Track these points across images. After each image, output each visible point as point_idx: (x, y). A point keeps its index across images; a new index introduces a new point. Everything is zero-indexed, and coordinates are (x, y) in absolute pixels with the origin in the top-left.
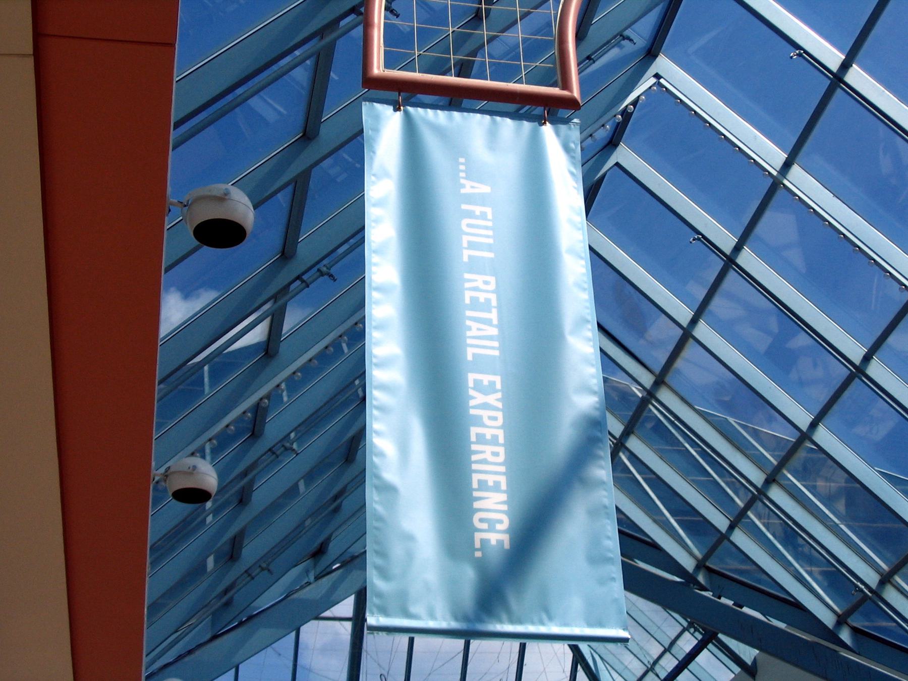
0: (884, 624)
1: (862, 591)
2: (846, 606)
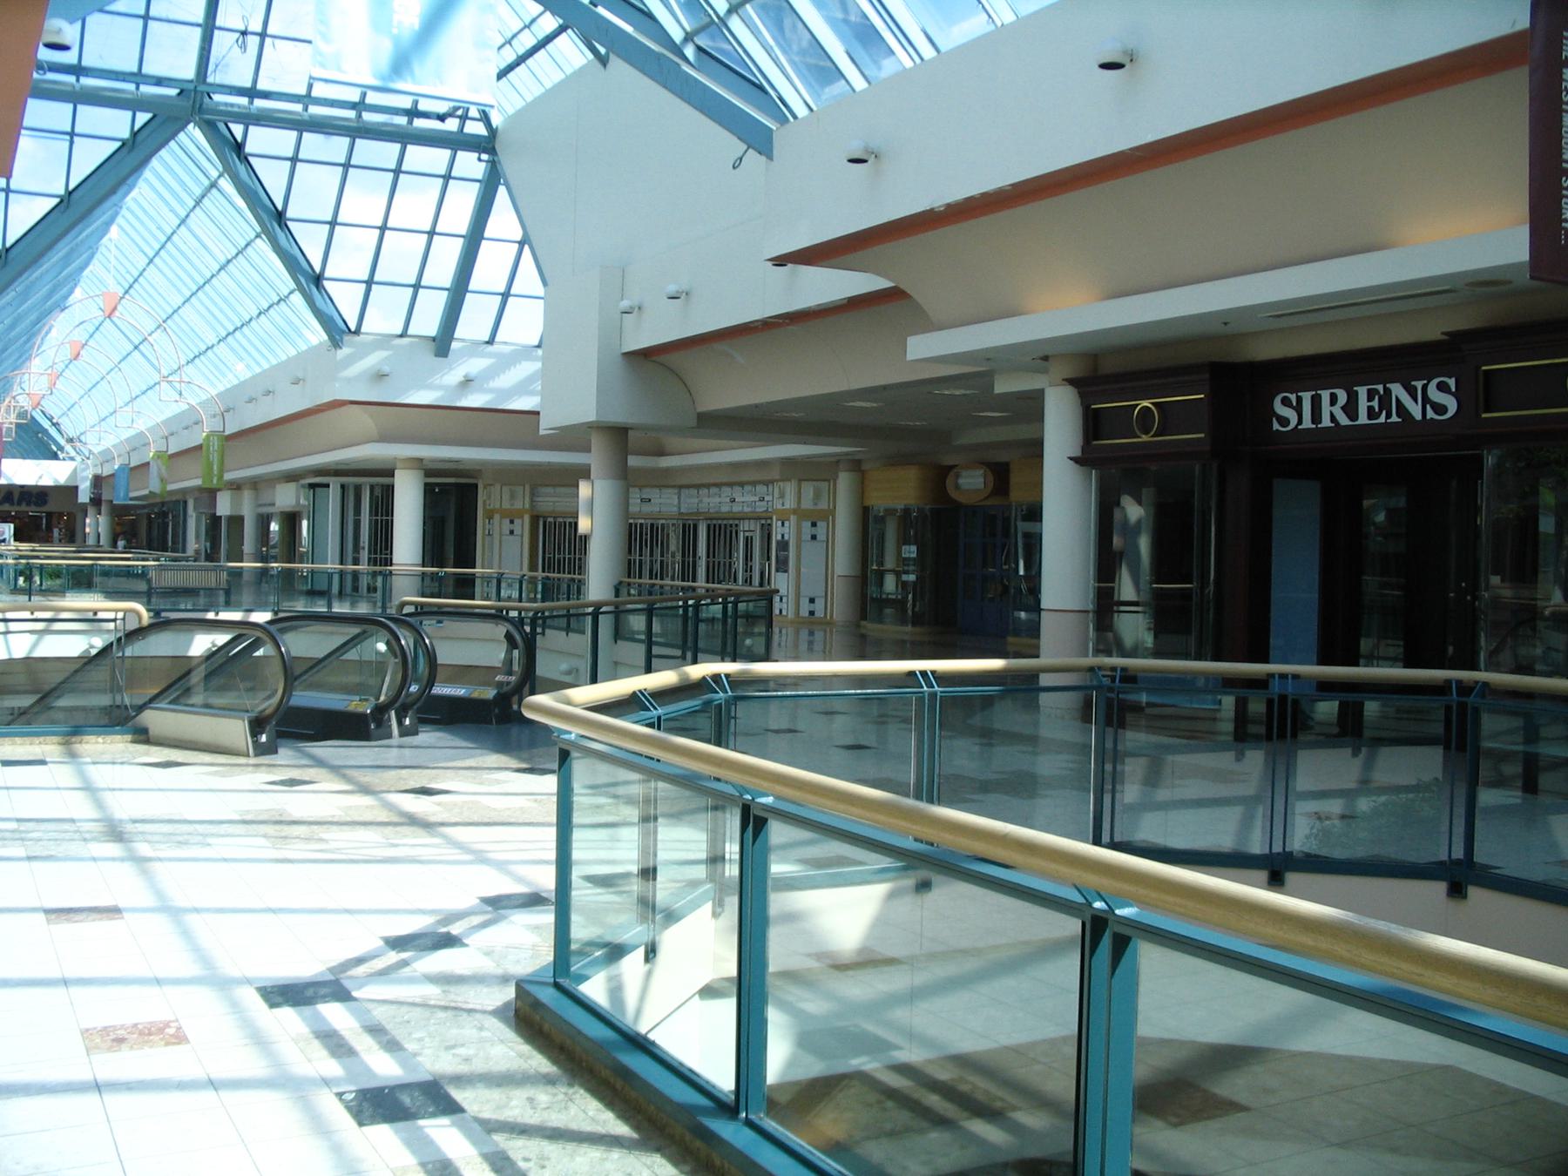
0: (726, 46)
1: (710, 16)
2: (696, 25)
